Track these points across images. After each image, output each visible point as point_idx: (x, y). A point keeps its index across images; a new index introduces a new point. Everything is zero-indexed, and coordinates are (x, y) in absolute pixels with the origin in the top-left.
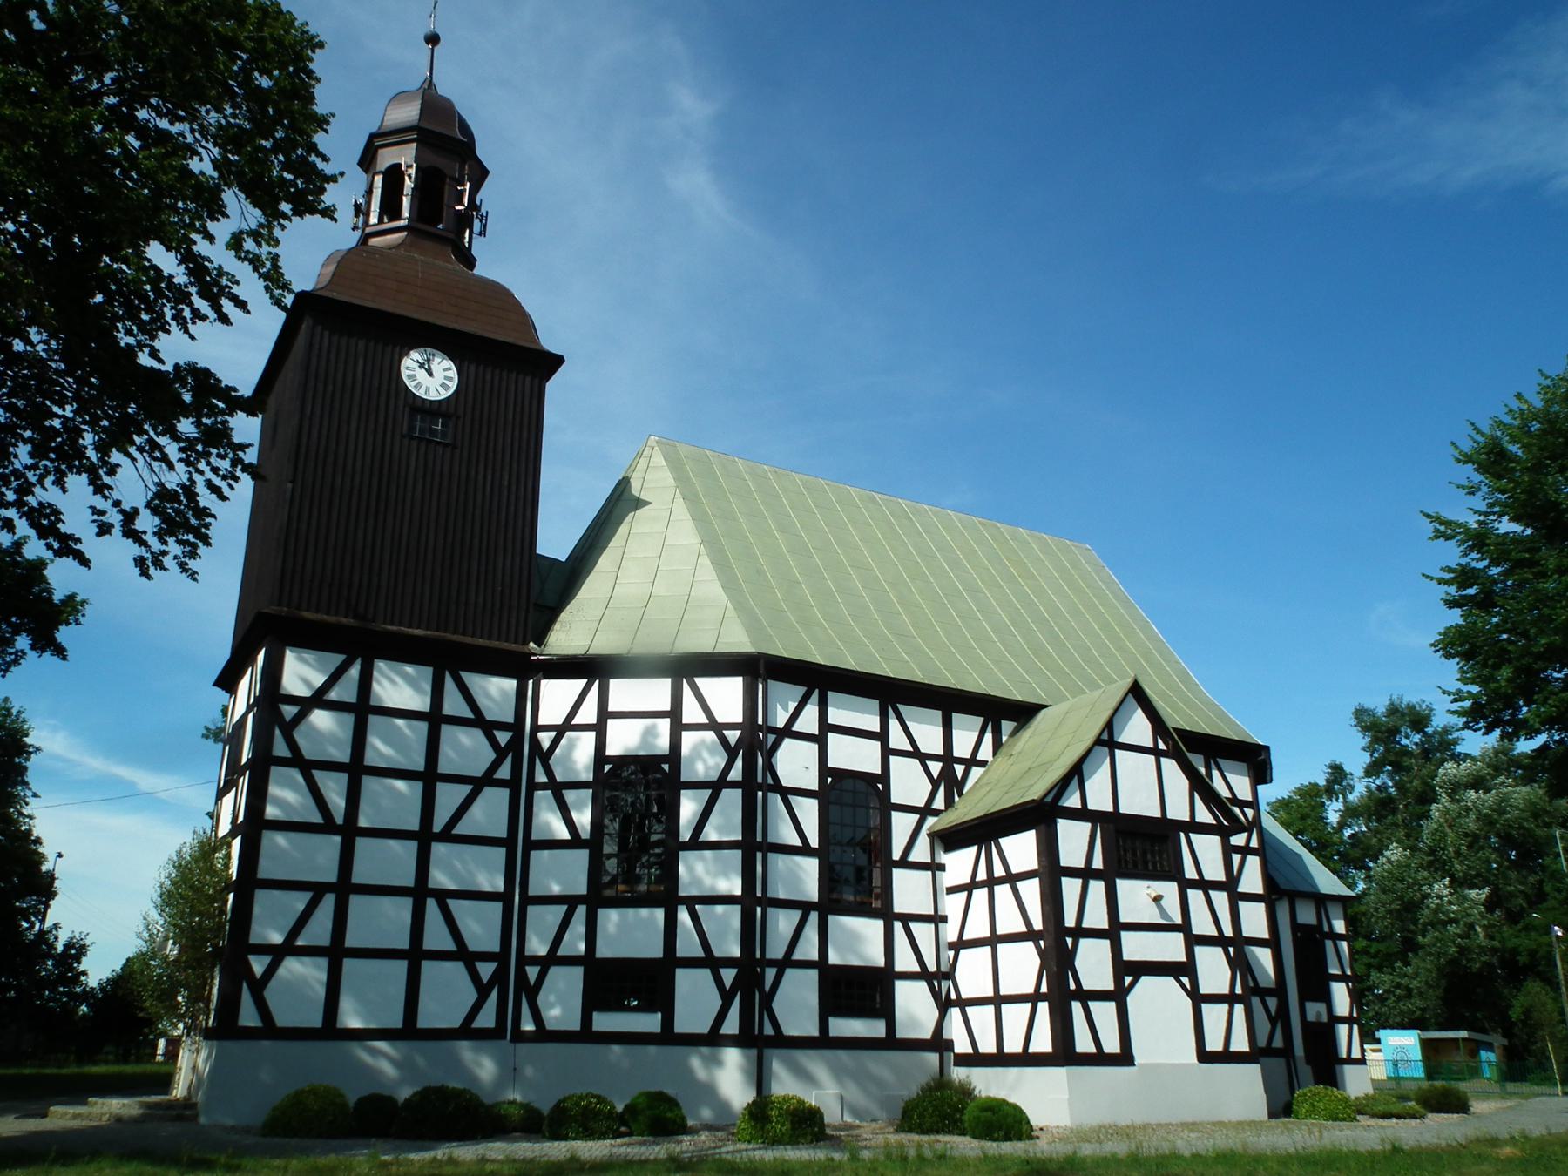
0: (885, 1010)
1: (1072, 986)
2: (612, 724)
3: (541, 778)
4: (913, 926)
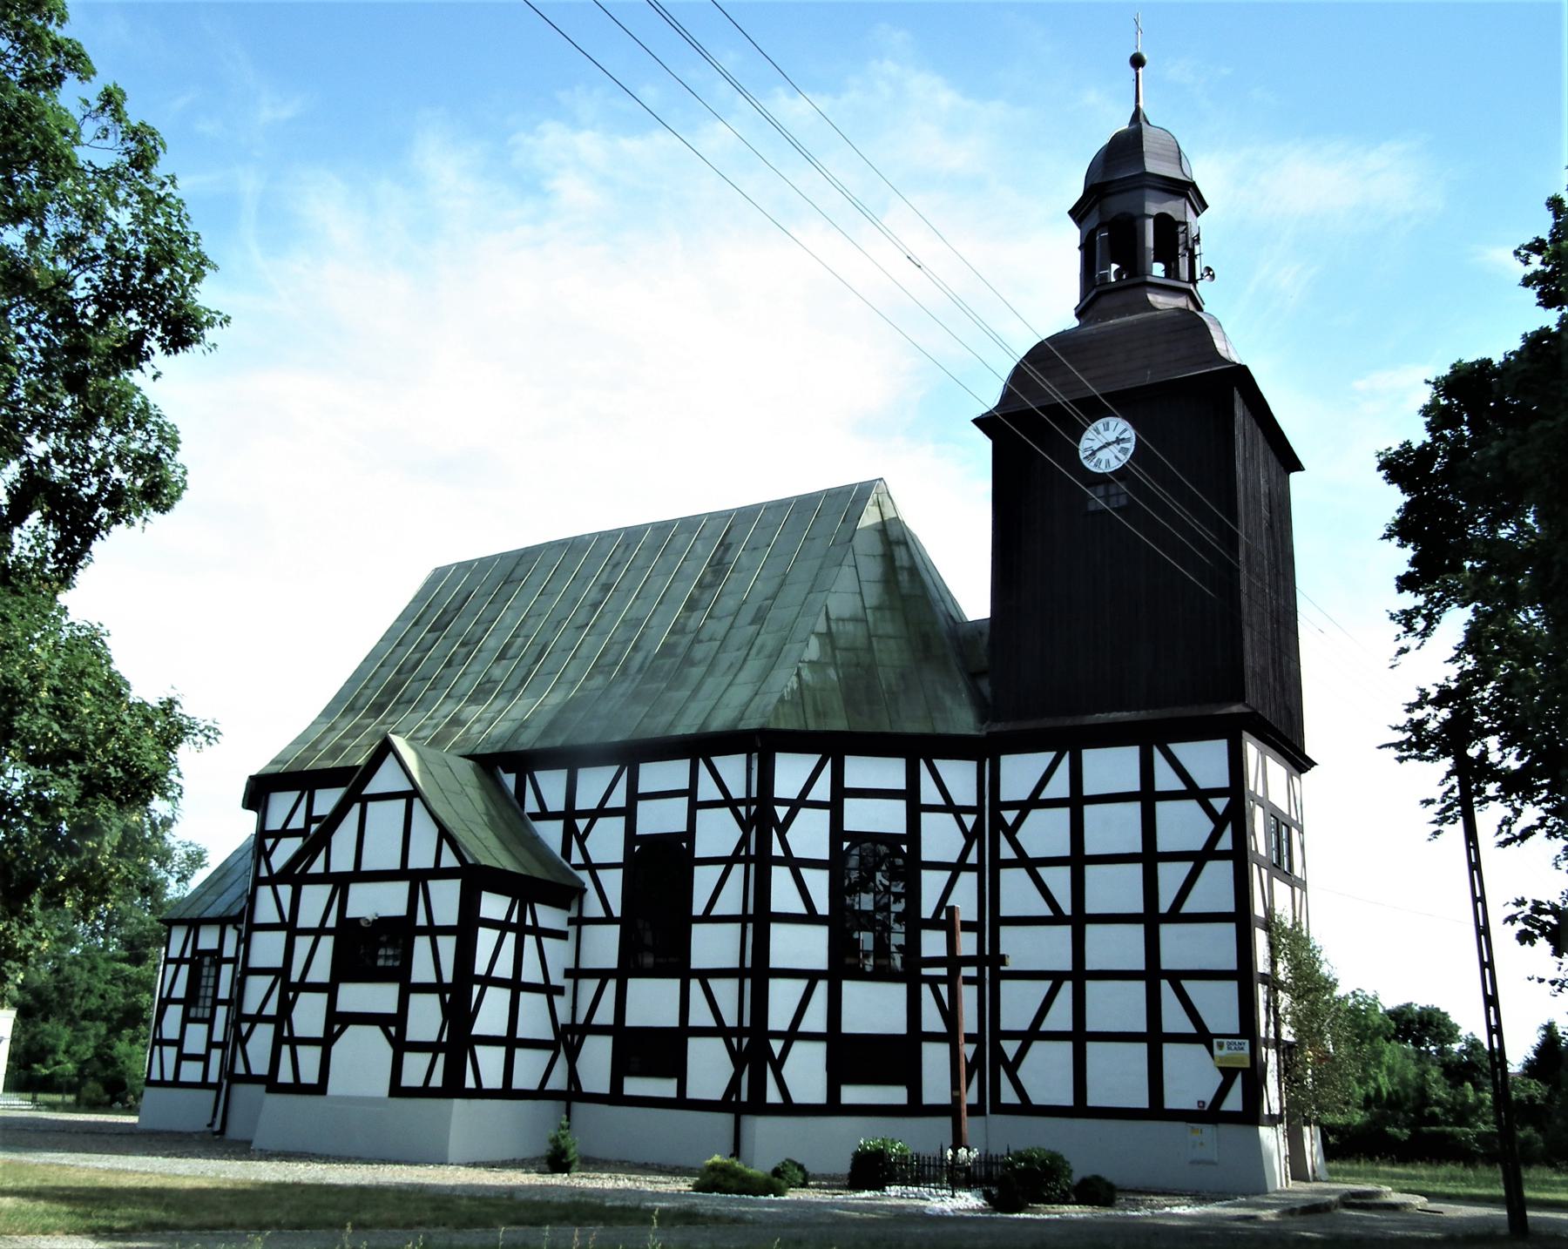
0: (676, 1067)
1: (286, 1034)
2: (642, 806)
3: (1006, 852)
4: (713, 983)
